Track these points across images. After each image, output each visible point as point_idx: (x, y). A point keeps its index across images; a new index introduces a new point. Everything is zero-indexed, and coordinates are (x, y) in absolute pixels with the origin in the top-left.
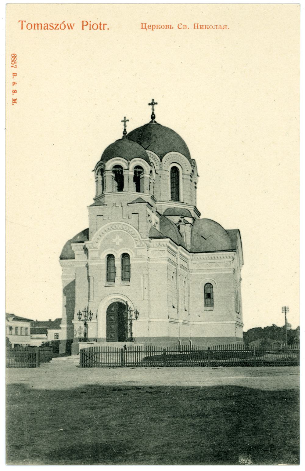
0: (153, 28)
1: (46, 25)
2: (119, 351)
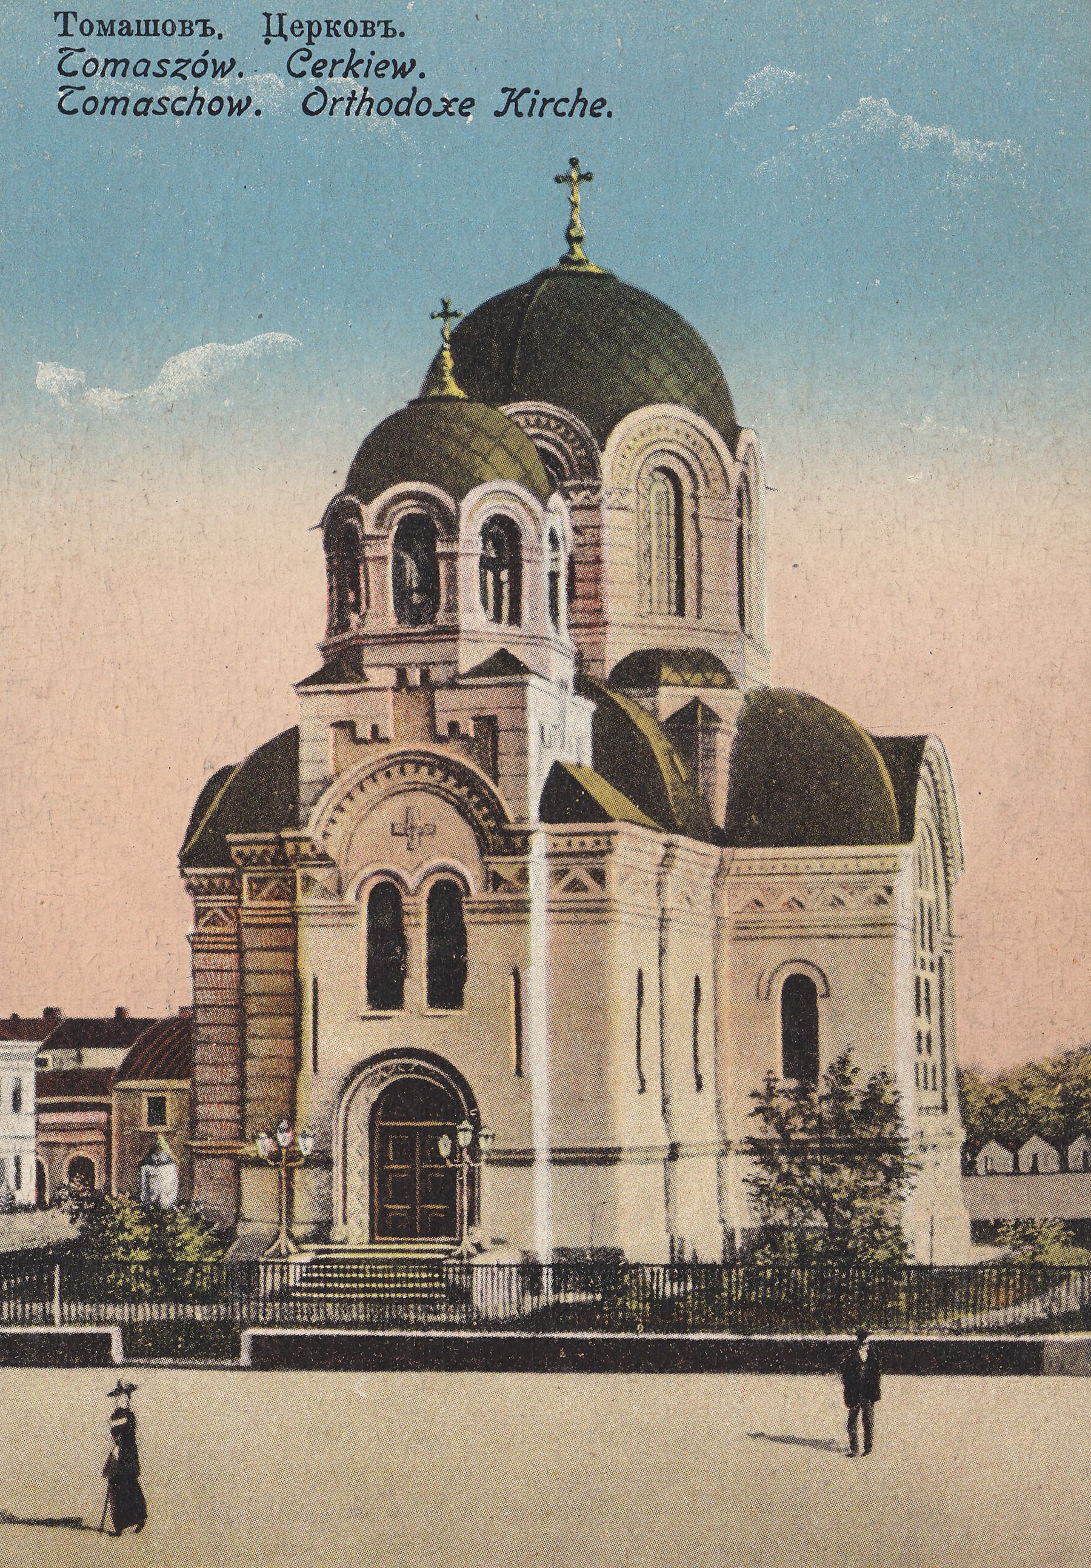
0: (310, 33)
1: (125, 24)
2: (235, 943)
